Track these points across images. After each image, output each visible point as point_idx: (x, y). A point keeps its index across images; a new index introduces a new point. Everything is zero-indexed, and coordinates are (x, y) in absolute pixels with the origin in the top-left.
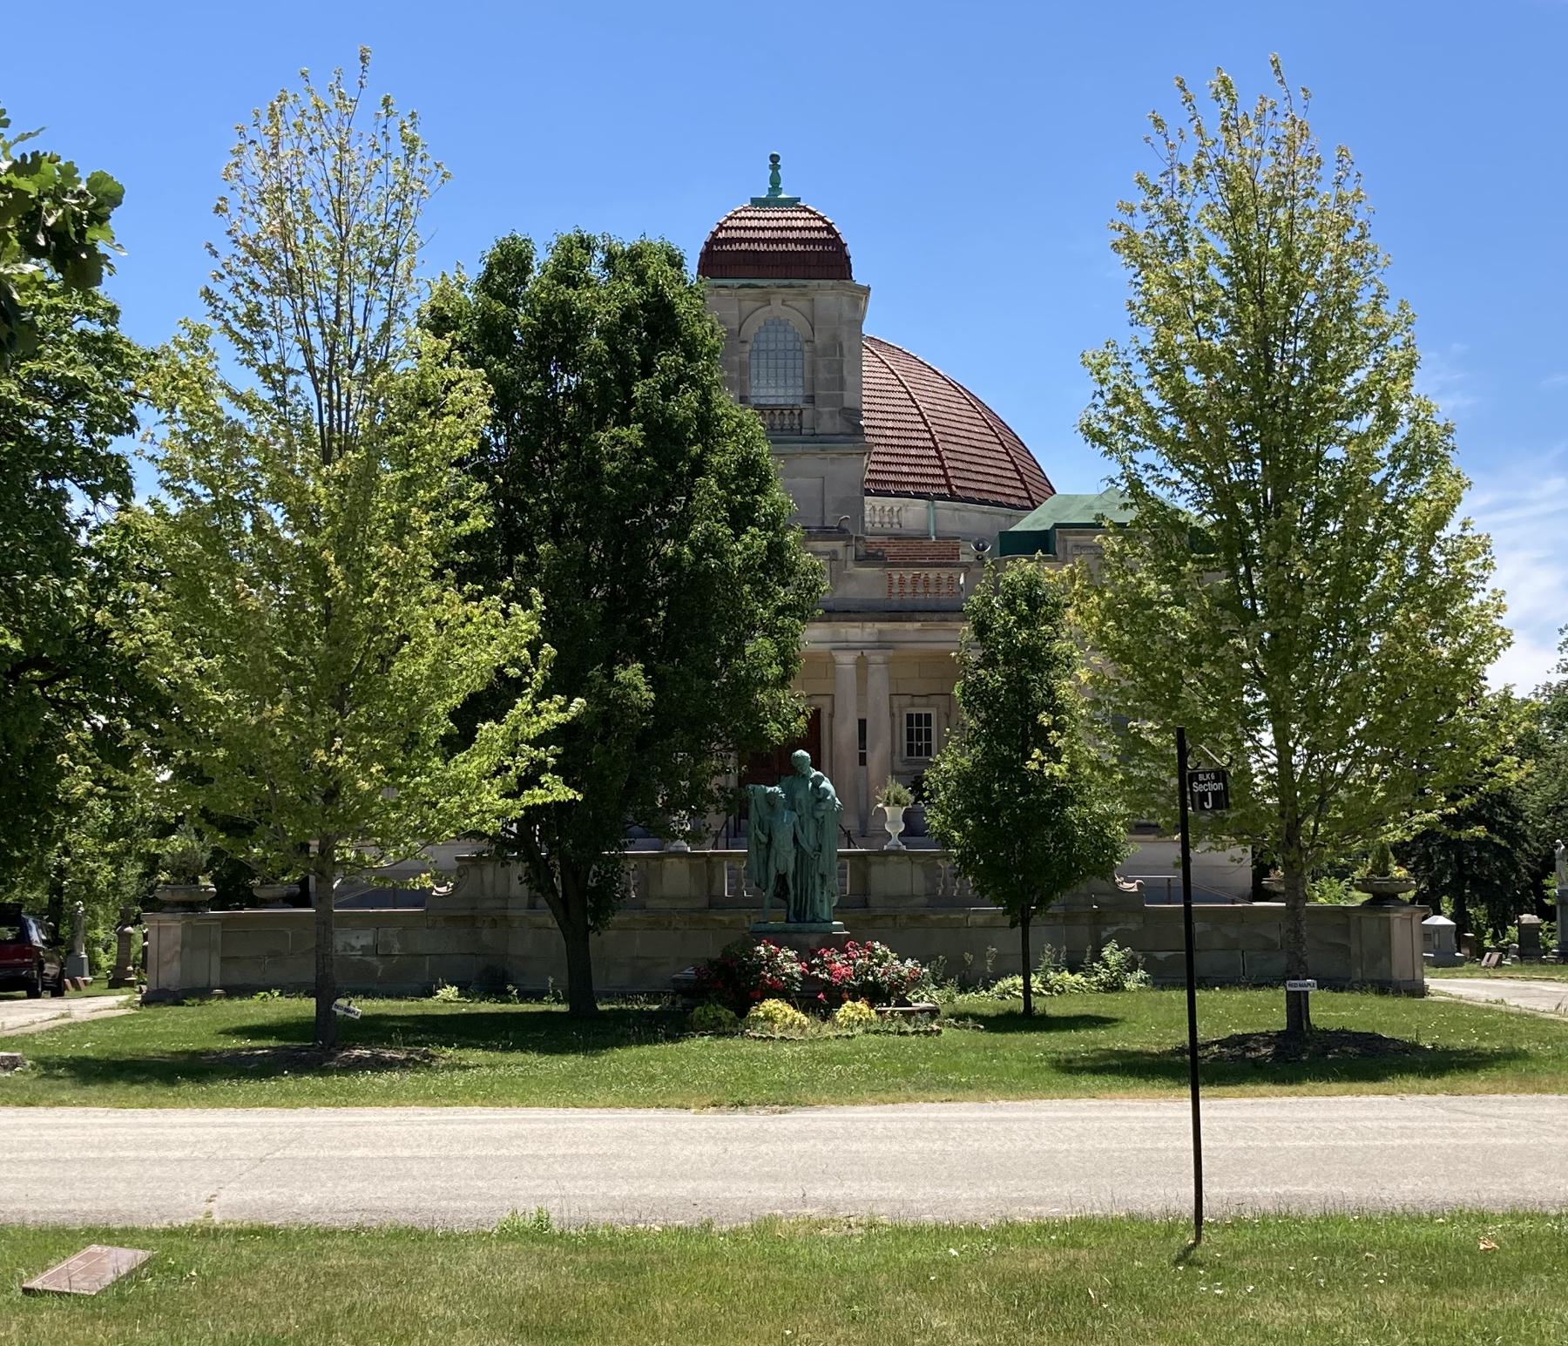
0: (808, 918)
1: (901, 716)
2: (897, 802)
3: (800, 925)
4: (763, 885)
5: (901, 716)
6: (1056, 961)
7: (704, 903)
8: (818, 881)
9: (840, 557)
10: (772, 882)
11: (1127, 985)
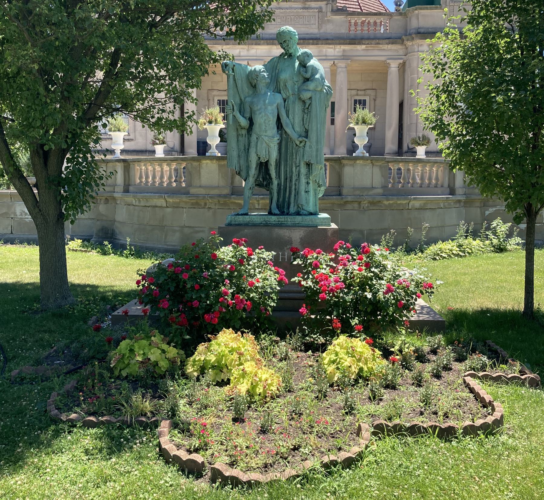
0: (292, 210)
1: (351, 100)
2: (364, 122)
3: (282, 218)
4: (244, 173)
5: (351, 100)
6: (467, 232)
7: (226, 191)
8: (303, 170)
9: (323, 11)
10: (253, 171)
11: (509, 247)
